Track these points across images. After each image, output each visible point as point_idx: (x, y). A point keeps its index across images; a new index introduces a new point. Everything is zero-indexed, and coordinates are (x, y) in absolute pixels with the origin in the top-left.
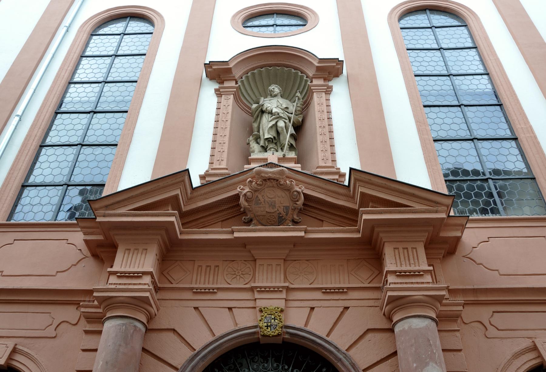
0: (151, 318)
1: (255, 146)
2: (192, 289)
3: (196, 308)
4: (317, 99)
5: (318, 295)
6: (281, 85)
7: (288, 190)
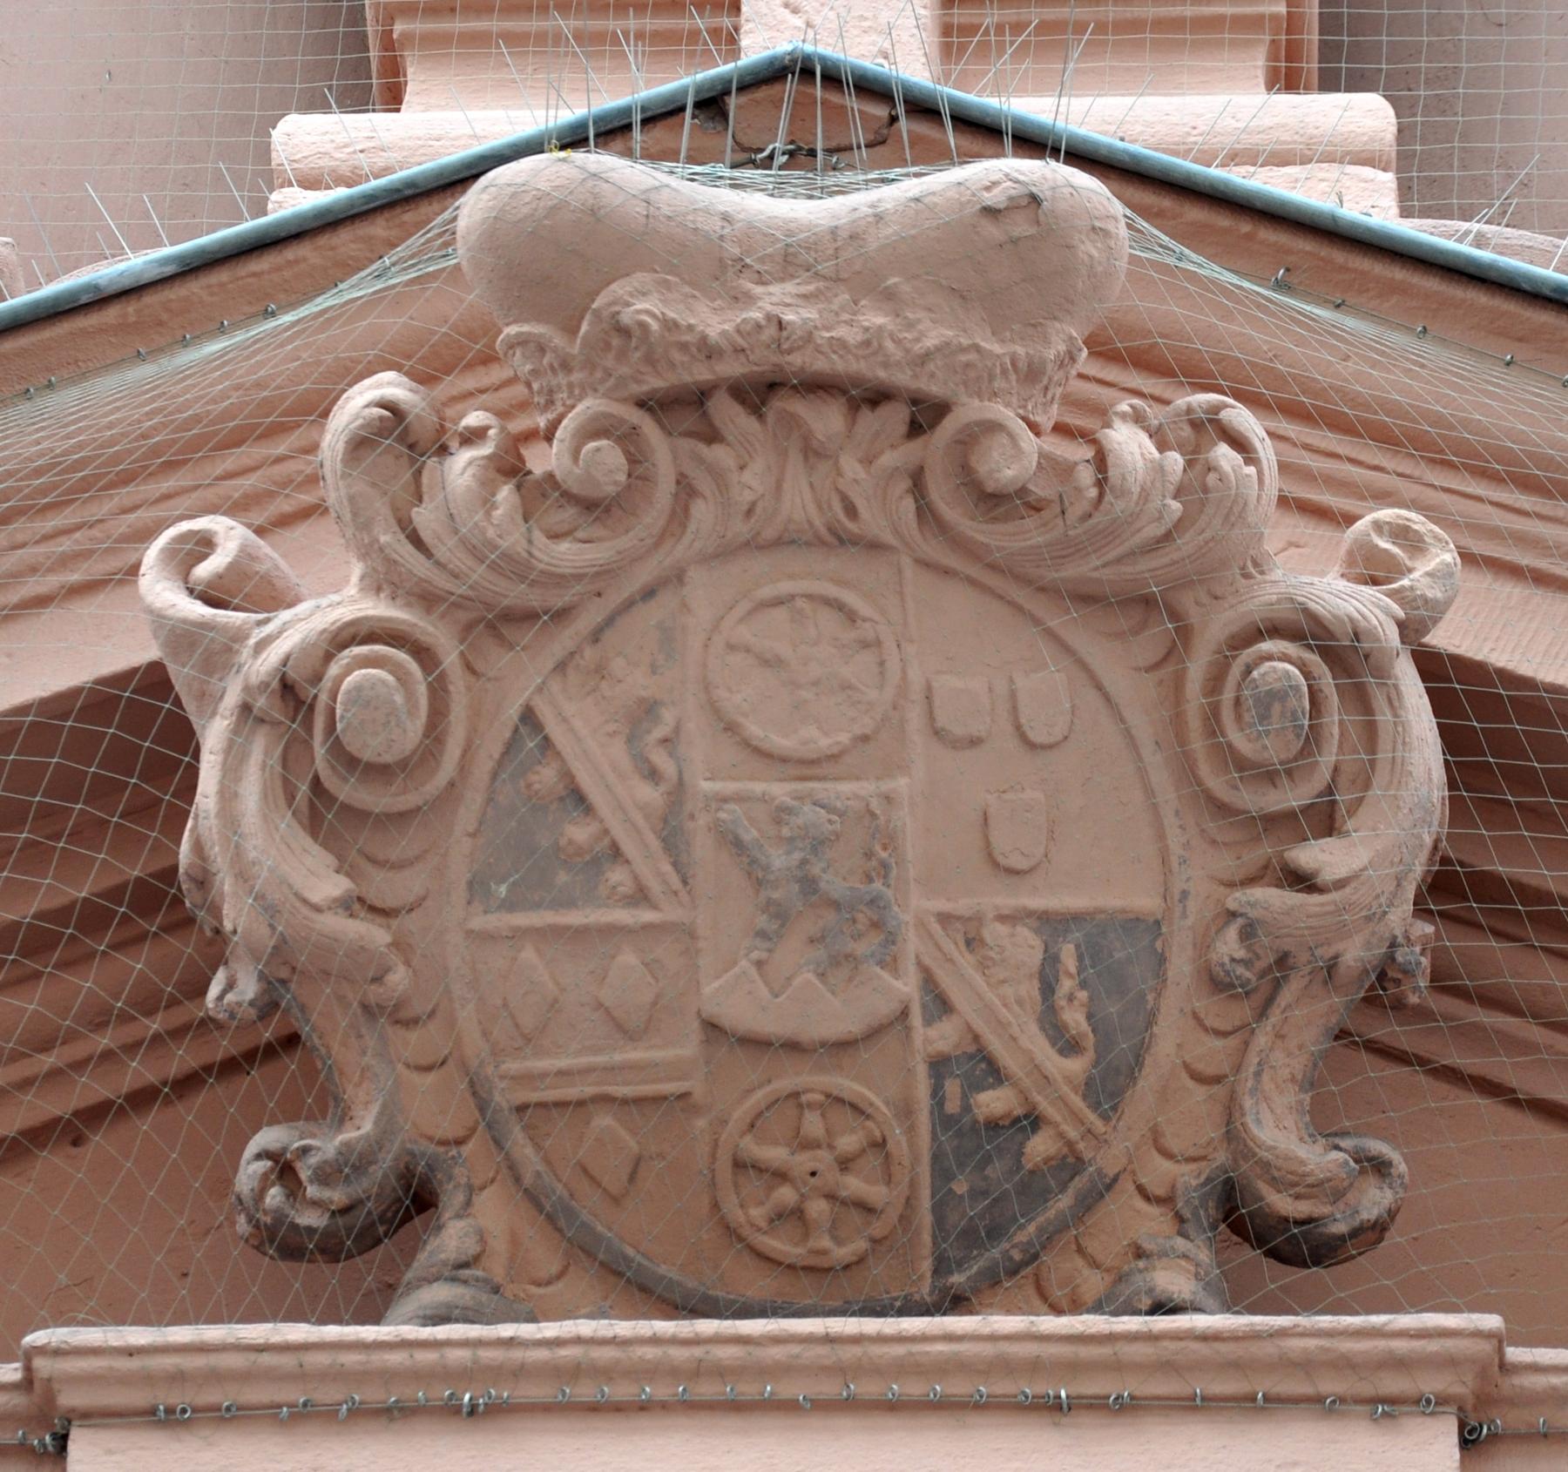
7: (1143, 596)
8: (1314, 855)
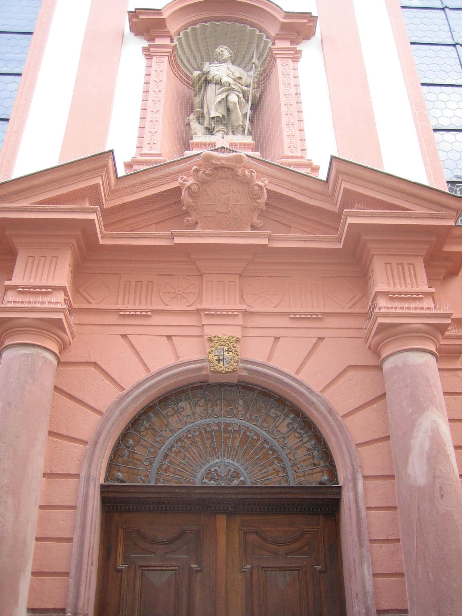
0: (64, 346)
1: (195, 126)
2: (119, 310)
3: (124, 336)
4: (281, 67)
5: (284, 322)
6: (231, 46)
7: (247, 182)
8: (258, 201)
